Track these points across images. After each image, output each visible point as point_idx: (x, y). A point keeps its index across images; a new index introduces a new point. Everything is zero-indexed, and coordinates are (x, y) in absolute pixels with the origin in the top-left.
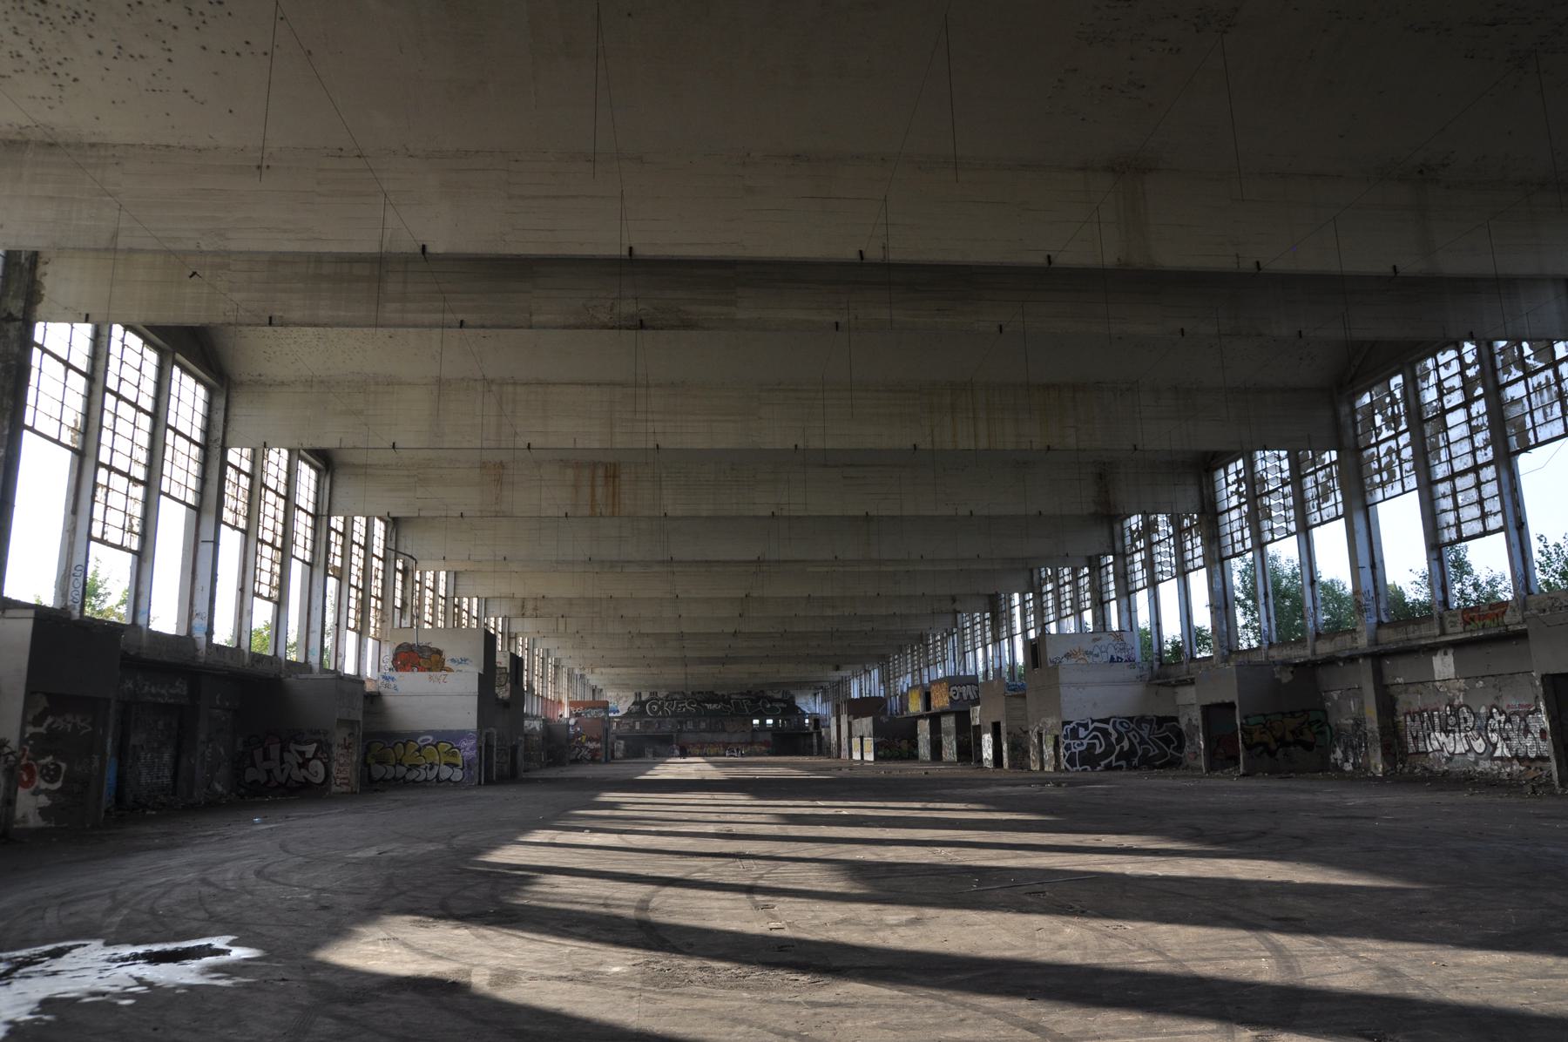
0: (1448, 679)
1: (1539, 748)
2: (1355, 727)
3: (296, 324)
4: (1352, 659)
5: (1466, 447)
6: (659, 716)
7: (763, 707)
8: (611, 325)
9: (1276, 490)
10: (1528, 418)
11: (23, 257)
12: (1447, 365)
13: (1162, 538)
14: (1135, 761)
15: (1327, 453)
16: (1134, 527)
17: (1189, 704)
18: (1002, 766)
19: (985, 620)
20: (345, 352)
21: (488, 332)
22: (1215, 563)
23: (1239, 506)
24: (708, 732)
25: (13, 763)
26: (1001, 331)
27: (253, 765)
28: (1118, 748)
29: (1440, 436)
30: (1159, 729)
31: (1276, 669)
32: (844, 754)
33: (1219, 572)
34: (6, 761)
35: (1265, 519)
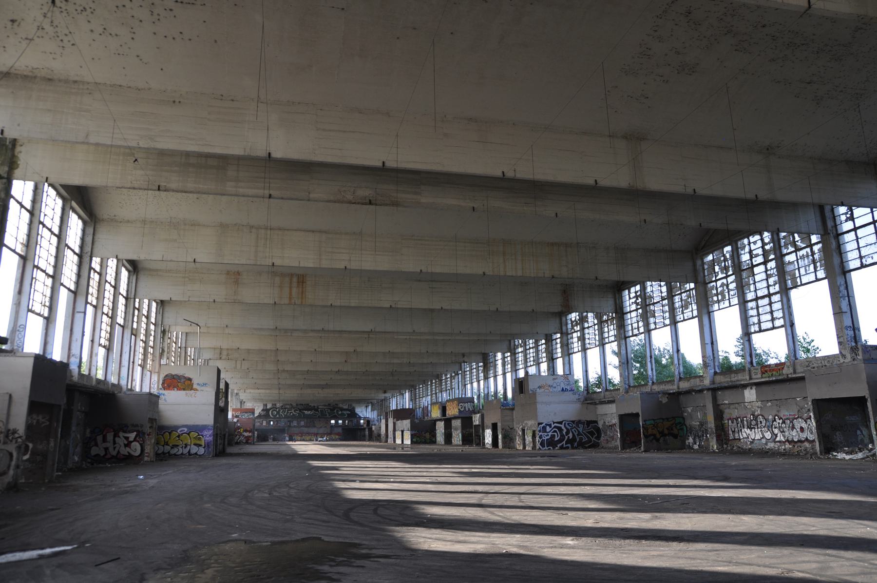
0: (753, 402)
1: (799, 436)
2: (700, 426)
3: (173, 191)
4: (701, 391)
5: (764, 284)
6: (277, 418)
7: (337, 413)
8: (353, 201)
9: (659, 302)
10: (797, 271)
11: (8, 141)
12: (755, 243)
13: (590, 326)
14: (576, 444)
15: (688, 284)
16: (573, 319)
17: (610, 414)
18: (498, 447)
19: (479, 367)
20: (169, 205)
21: (255, 199)
22: (622, 339)
23: (637, 310)
24: (306, 427)
25: (20, 443)
26: (557, 216)
27: (96, 445)
28: (566, 437)
29: (750, 278)
30: (587, 427)
31: (660, 396)
32: (390, 441)
33: (624, 344)
34: (16, 442)
35: (651, 317)
